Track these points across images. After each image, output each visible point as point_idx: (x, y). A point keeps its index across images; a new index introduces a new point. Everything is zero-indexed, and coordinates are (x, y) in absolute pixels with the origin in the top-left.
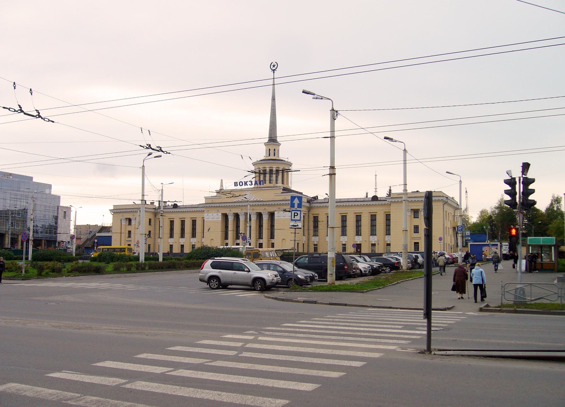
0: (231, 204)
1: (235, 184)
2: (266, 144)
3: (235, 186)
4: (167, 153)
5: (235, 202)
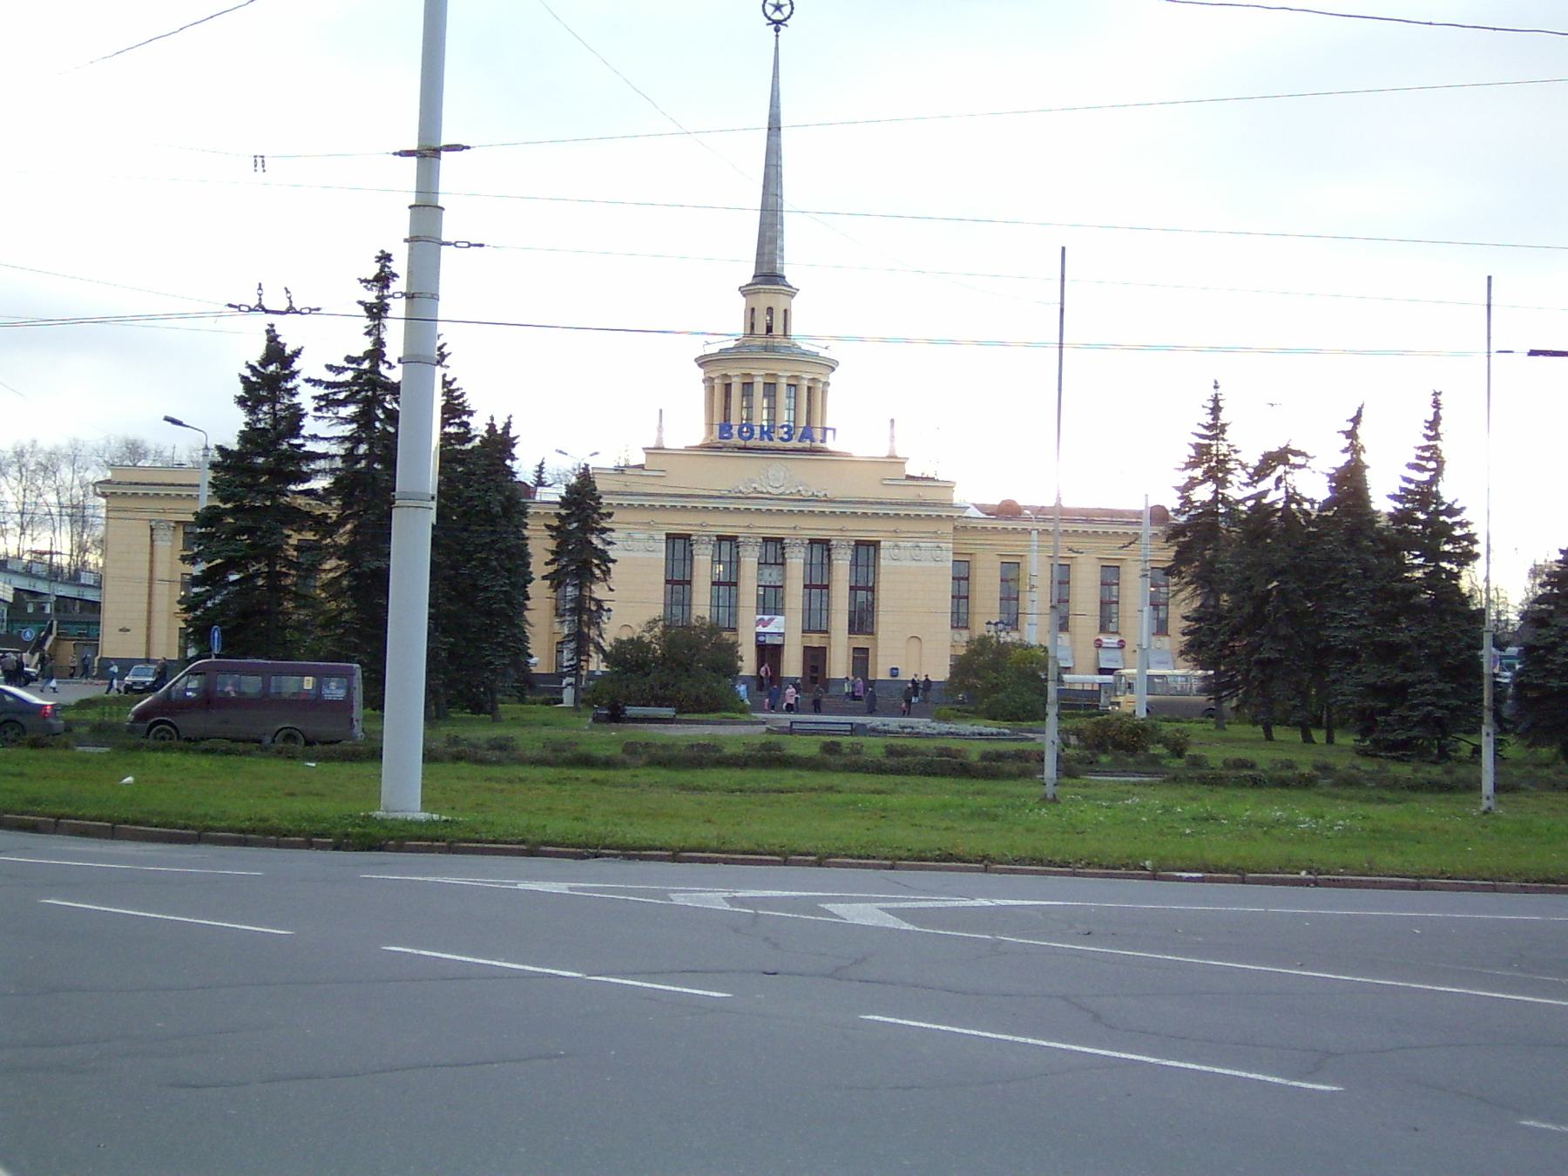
2: (746, 291)
4: (260, 295)
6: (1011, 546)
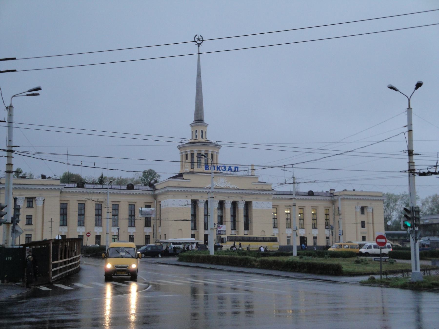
0: (189, 190)
2: (191, 125)
3: (206, 169)
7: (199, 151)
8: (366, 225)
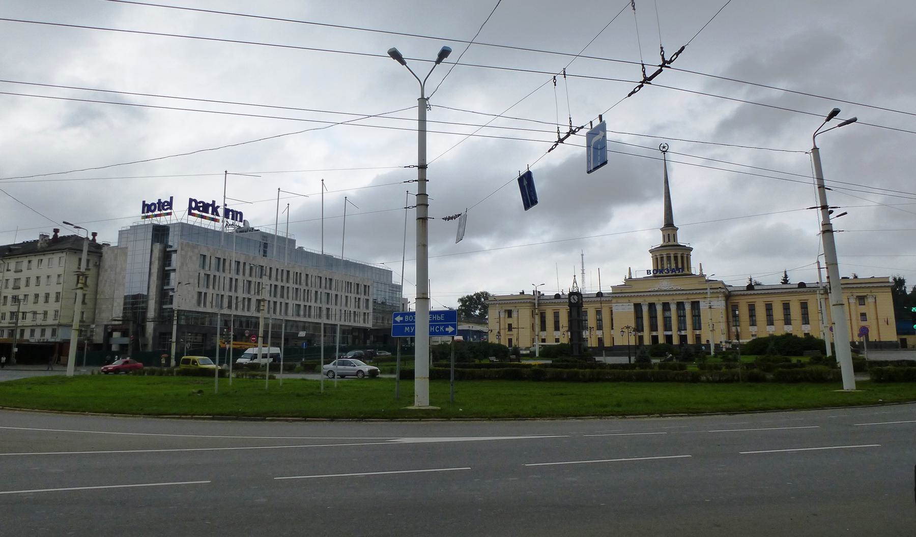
1: (648, 272)
2: (662, 229)
3: (648, 274)
5: (650, 291)
6: (751, 299)
7: (667, 254)
8: (507, 327)
